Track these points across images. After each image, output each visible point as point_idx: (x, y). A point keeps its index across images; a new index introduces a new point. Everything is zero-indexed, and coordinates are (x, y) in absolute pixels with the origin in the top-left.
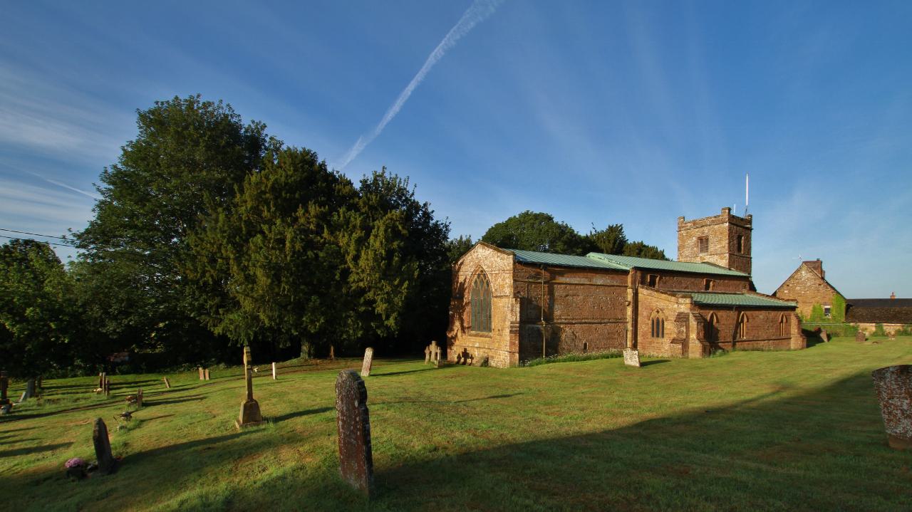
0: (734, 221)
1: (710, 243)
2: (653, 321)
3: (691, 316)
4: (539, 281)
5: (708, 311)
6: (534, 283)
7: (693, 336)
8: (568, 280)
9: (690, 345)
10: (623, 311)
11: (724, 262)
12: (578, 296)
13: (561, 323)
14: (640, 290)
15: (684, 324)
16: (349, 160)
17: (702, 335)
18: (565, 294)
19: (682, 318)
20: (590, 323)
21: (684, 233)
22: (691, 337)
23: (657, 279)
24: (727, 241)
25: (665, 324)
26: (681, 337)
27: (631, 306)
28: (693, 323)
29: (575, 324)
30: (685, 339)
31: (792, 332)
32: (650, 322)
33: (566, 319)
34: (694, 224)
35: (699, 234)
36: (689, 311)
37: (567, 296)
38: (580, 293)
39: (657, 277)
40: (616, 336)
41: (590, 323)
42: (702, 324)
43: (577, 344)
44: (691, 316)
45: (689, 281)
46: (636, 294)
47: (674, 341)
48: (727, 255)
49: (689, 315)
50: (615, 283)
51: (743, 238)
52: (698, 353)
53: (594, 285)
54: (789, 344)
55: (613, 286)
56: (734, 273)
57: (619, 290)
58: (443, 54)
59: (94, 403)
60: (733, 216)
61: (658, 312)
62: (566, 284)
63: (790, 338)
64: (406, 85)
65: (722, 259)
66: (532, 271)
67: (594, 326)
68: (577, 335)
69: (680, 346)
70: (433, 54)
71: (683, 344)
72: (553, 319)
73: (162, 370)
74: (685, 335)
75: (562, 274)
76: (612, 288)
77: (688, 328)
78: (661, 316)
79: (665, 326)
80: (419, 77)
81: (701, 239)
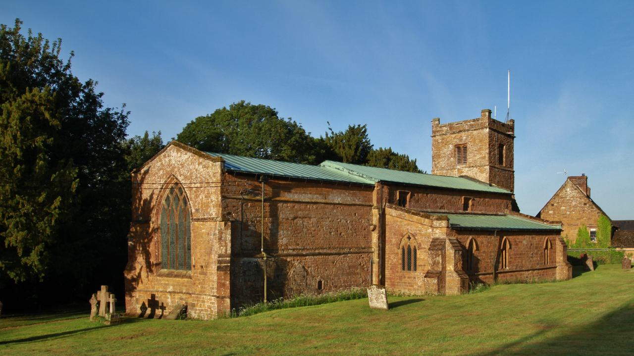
1: (468, 152)
4: (258, 198)
5: (466, 236)
7: (450, 267)
10: (367, 237)
11: (484, 176)
12: (310, 218)
14: (388, 210)
17: (460, 266)
18: (292, 216)
19: (437, 246)
24: (487, 151)
26: (436, 269)
28: (450, 251)
30: (441, 272)
31: (557, 260)
32: (400, 251)
33: (294, 250)
34: (451, 128)
36: (445, 237)
37: (295, 218)
42: (461, 253)
43: (308, 282)
46: (382, 216)
47: (428, 275)
48: (488, 168)
49: (445, 242)
51: (505, 147)
52: (456, 289)
54: (554, 274)
55: (354, 205)
61: (409, 238)
63: (556, 267)
65: (482, 172)
66: (247, 184)
67: (331, 257)
68: (309, 271)
72: (277, 250)
75: (288, 189)
79: (418, 256)
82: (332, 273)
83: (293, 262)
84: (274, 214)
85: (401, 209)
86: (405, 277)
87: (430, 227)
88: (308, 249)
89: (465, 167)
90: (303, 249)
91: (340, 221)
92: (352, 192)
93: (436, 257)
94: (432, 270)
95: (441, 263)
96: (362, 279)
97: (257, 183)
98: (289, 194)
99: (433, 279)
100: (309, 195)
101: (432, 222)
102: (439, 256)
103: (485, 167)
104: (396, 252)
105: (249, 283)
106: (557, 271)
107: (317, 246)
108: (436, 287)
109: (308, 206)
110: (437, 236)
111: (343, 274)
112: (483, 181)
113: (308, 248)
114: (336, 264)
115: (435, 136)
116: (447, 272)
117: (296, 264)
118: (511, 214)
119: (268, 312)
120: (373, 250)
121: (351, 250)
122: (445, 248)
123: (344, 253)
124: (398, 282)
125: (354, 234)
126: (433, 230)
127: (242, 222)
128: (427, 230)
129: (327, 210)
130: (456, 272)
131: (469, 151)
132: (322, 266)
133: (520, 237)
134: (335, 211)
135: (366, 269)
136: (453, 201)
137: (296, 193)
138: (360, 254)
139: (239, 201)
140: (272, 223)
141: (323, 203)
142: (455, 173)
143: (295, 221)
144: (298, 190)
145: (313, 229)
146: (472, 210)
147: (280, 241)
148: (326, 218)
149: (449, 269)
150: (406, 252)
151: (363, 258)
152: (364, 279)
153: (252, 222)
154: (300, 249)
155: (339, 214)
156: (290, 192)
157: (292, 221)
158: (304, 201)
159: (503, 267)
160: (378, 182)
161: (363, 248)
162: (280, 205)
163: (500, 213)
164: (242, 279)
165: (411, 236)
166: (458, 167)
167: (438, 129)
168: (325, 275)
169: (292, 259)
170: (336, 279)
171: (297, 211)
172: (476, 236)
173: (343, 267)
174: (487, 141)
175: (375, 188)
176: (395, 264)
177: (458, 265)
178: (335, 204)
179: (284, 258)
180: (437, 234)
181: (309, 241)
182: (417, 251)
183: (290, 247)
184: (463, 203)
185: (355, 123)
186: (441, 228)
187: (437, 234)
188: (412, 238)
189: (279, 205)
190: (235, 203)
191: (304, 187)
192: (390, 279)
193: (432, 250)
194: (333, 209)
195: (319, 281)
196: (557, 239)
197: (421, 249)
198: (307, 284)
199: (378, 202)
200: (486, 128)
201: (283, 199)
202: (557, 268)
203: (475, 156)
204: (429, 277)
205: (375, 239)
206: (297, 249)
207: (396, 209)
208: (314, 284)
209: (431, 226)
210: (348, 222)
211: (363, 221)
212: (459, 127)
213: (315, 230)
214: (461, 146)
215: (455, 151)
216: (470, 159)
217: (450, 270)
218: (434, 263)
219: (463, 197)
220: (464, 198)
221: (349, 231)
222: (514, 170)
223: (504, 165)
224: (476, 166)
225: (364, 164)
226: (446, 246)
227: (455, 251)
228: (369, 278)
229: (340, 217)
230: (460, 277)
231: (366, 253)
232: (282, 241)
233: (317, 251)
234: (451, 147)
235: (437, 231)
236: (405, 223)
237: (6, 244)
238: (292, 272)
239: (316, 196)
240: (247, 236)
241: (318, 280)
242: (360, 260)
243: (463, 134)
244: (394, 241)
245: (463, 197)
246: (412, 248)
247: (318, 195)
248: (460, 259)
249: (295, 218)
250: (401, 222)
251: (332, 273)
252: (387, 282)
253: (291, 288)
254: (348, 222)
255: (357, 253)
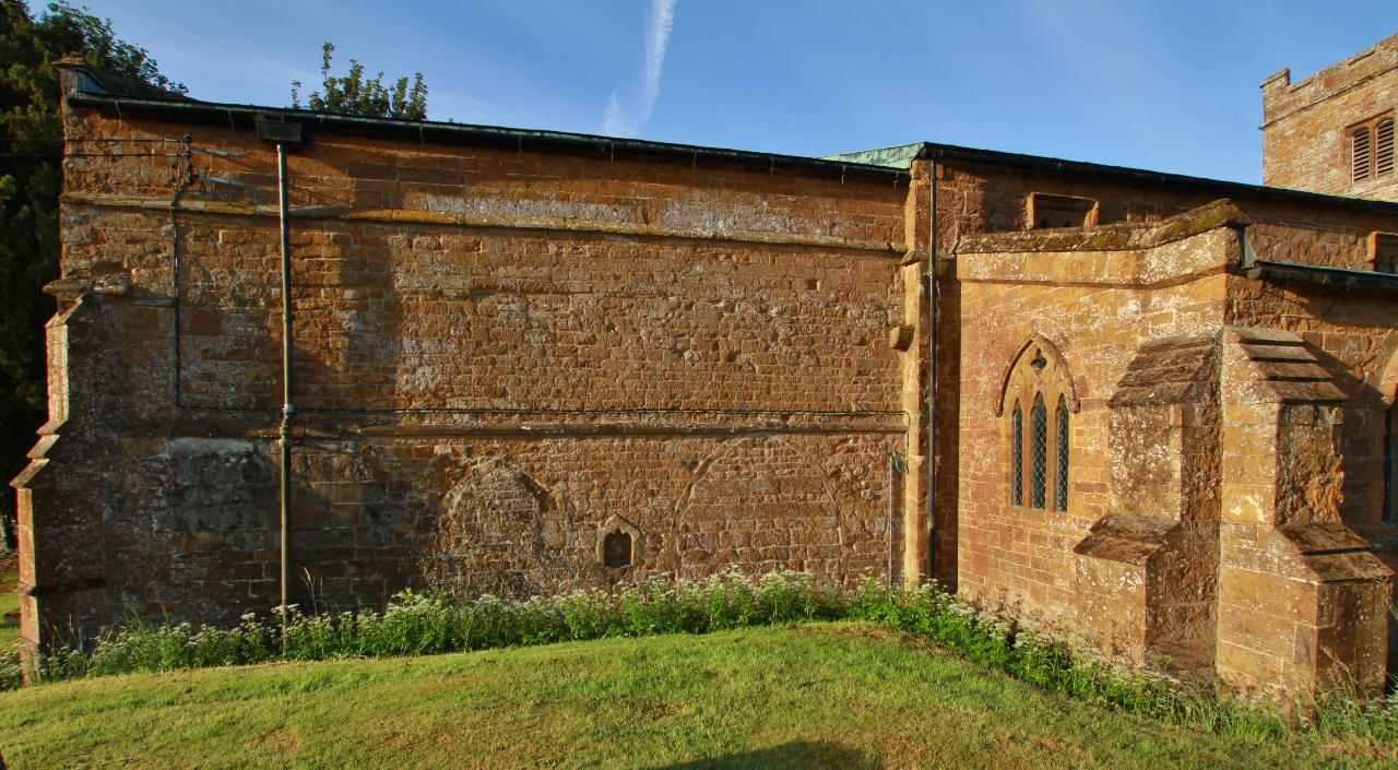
2: (1017, 413)
3: (1232, 356)
7: (1248, 504)
8: (483, 210)
9: (1227, 571)
10: (875, 373)
12: (564, 293)
14: (974, 266)
15: (1173, 415)
17: (1323, 496)
18: (460, 283)
19: (1173, 383)
20: (647, 433)
21: (1287, 126)
22: (1232, 510)
25: (1073, 428)
26: (1149, 508)
27: (915, 348)
28: (1248, 411)
29: (537, 435)
30: (1174, 533)
32: (1005, 424)
33: (477, 413)
34: (1329, 84)
36: (1214, 326)
37: (479, 292)
38: (575, 280)
40: (826, 499)
41: (647, 433)
42: (1331, 417)
43: (550, 536)
44: (1232, 356)
46: (943, 288)
47: (1100, 541)
49: (1211, 358)
50: (818, 236)
52: (1290, 642)
53: (673, 239)
55: (807, 248)
57: (846, 271)
61: (1039, 362)
68: (556, 492)
69: (1139, 580)
71: (1153, 563)
74: (1175, 497)
76: (799, 259)
77: (1203, 447)
78: (1052, 383)
79: (1073, 440)
81: (1358, 132)
82: (685, 504)
83: (464, 460)
85: (1008, 242)
86: (1020, 536)
87: (1129, 293)
88: (556, 413)
89: (1387, 184)
90: (525, 415)
93: (1148, 445)
94: (1124, 513)
95: (1177, 475)
96: (847, 530)
97: (260, 155)
99: (1120, 566)
101: (1141, 257)
102: (1167, 433)
104: (992, 426)
105: (204, 536)
108: (1134, 616)
109: (553, 248)
110: (1168, 330)
111: (740, 511)
113: (555, 407)
114: (701, 473)
115: (1271, 124)
116: (1226, 530)
117: (482, 467)
119: (178, 674)
120: (905, 419)
121: (791, 421)
122: (1214, 393)
123: (742, 432)
124: (998, 553)
125: (806, 360)
126: (1145, 306)
128: (1115, 314)
129: (656, 266)
130: (1292, 535)
132: (629, 477)
134: (699, 268)
135: (866, 494)
136: (1324, 247)
138: (836, 438)
139: (162, 222)
143: (484, 303)
145: (583, 335)
147: (403, 381)
148: (652, 296)
149: (1237, 511)
150: (1027, 419)
151: (851, 450)
152: (855, 529)
153: (241, 302)
154: (511, 412)
155: (721, 280)
157: (467, 305)
160: (918, 157)
164: (162, 521)
165: (1044, 354)
167: (1286, 100)
168: (647, 511)
169: (461, 448)
171: (490, 266)
173: (742, 482)
175: (912, 184)
176: (987, 477)
177: (1313, 494)
178: (697, 241)
180: (1167, 317)
181: (560, 383)
182: (1072, 416)
183: (453, 403)
186: (1190, 279)
187: (1167, 317)
188: (1050, 361)
190: (130, 224)
192: (973, 535)
193: (1131, 405)
194: (689, 262)
195: (609, 538)
197: (1089, 405)
199: (920, 233)
204: (1099, 555)
205: (910, 381)
206: (495, 412)
207: (988, 249)
209: (1137, 286)
210: (773, 312)
211: (853, 311)
212: (1360, 68)
213: (592, 340)
215: (1345, 146)
217: (1247, 519)
218: (1139, 478)
219: (1371, 239)
220: (1378, 236)
221: (780, 349)
226: (1224, 379)
227: (1287, 404)
228: (880, 525)
229: (725, 293)
230: (1322, 570)
231: (869, 432)
232: (417, 376)
233: (603, 421)
234: (1331, 137)
235: (1170, 302)
236: (1024, 300)
238: (458, 498)
239: (592, 207)
240: (208, 354)
241: (602, 530)
242: (837, 459)
244: (984, 379)
245: (1371, 239)
246: (1051, 409)
248: (1322, 459)
249: (479, 292)
250: (1009, 298)
251: (685, 504)
252: (964, 546)
253: (451, 561)
254: (773, 312)
255: (814, 430)
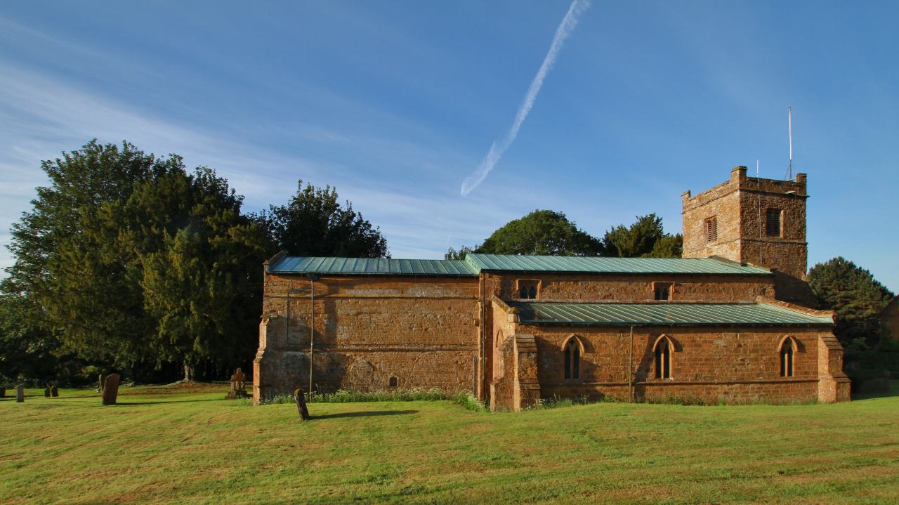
0: (751, 187)
1: (718, 226)
4: (308, 295)
5: (562, 334)
6: (299, 298)
8: (360, 293)
11: (734, 254)
13: (349, 350)
16: (486, 172)
18: (354, 312)
20: (402, 350)
21: (689, 214)
23: (539, 286)
24: (739, 220)
31: (820, 370)
33: (357, 345)
35: (706, 215)
37: (358, 314)
38: (383, 309)
39: (669, 285)
41: (402, 350)
43: (375, 378)
45: (614, 286)
48: (739, 242)
50: (452, 295)
51: (782, 212)
54: (815, 390)
55: (448, 298)
56: (752, 269)
58: (575, 22)
59: (134, 409)
60: (754, 180)
62: (355, 298)
63: (818, 381)
64: (537, 70)
65: (732, 249)
66: (298, 284)
67: (409, 354)
68: (377, 366)
70: (562, 26)
72: (336, 345)
73: (84, 386)
75: (350, 286)
80: (548, 60)
82: (412, 370)
84: (331, 311)
90: (370, 345)
91: (426, 316)
92: (444, 284)
97: (307, 282)
98: (351, 290)
100: (378, 290)
103: (735, 242)
106: (819, 388)
107: (391, 342)
109: (377, 302)
111: (428, 372)
112: (733, 260)
118: (764, 302)
121: (444, 347)
127: (288, 319)
131: (719, 223)
133: (707, 336)
137: (360, 289)
140: (329, 318)
141: (399, 298)
142: (705, 254)
143: (359, 317)
144: (363, 286)
146: (674, 298)
147: (339, 337)
151: (461, 355)
156: (353, 288)
157: (355, 317)
158: (369, 296)
159: (658, 375)
161: (463, 345)
162: (338, 302)
163: (741, 302)
164: (284, 371)
166: (708, 246)
168: (401, 372)
170: (418, 377)
172: (588, 334)
173: (429, 364)
174: (738, 208)
178: (416, 298)
179: (343, 353)
183: (351, 342)
184: (653, 289)
185: (645, 214)
189: (336, 301)
191: (370, 283)
194: (414, 304)
195: (391, 379)
196: (820, 338)
198: (373, 380)
200: (736, 190)
201: (344, 295)
202: (820, 383)
203: (725, 229)
206: (362, 345)
208: (383, 380)
210: (438, 317)
213: (387, 326)
214: (712, 219)
215: (705, 227)
216: (721, 234)
219: (653, 283)
222: (807, 241)
223: (781, 236)
224: (726, 243)
225: (645, 254)
232: (342, 334)
233: (390, 347)
234: (701, 222)
237: (171, 341)
239: (388, 290)
240: (294, 331)
241: (389, 377)
243: (712, 204)
245: (653, 283)
247: (391, 290)
249: (358, 314)
251: (412, 370)
253: (350, 384)
254: (438, 317)
